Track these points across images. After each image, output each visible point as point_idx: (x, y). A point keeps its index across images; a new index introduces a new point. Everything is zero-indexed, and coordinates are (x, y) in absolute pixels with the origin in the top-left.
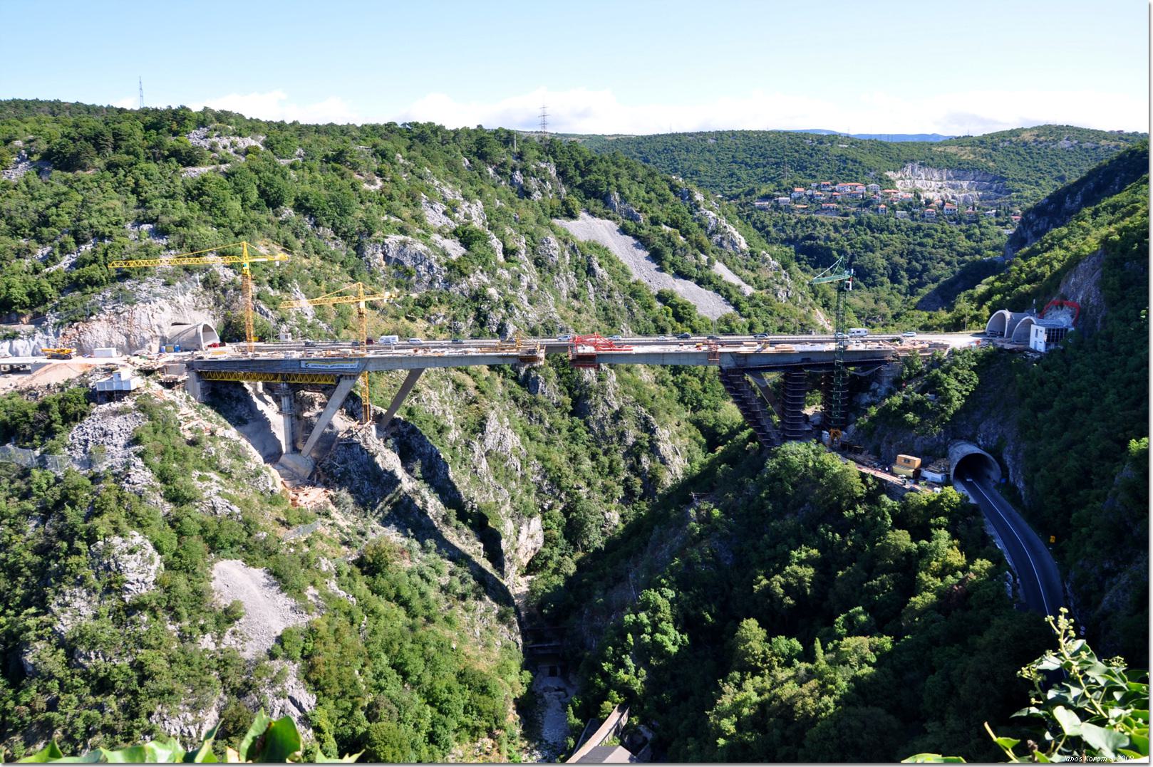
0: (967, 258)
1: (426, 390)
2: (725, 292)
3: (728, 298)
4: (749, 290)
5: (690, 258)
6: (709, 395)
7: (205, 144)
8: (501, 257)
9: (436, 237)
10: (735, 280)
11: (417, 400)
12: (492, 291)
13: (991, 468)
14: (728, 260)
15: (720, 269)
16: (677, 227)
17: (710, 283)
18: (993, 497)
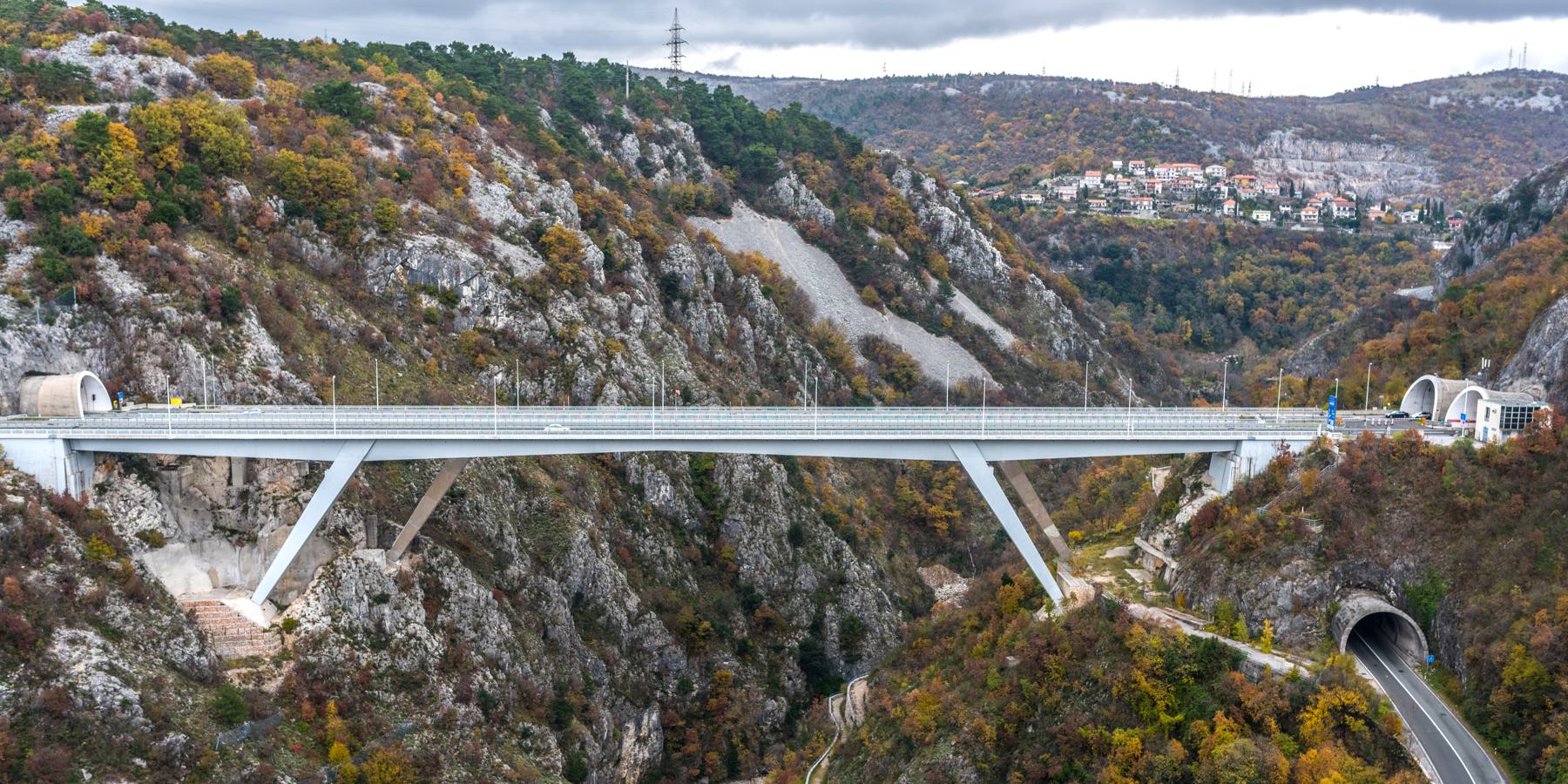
2: (975, 342)
4: (1006, 339)
7: (94, 66)
10: (985, 322)
12: (585, 333)
15: (962, 303)
18: (1415, 687)
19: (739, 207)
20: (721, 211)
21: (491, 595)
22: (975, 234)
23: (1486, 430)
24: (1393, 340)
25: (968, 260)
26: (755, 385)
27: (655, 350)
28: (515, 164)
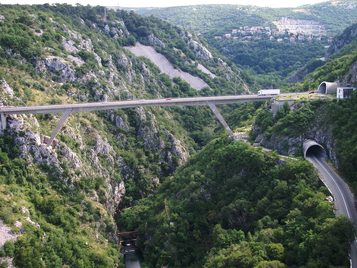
1: (68, 127)
3: (204, 79)
4: (213, 76)
5: (187, 63)
6: (198, 124)
8: (100, 65)
9: (71, 57)
11: (65, 132)
14: (204, 63)
15: (200, 67)
16: (181, 49)
17: (196, 73)
19: (138, 44)
20: (132, 44)
21: (76, 155)
22: (204, 49)
23: (339, 95)
24: (315, 73)
25: (202, 55)
26: (145, 92)
27: (116, 84)
28: (75, 35)
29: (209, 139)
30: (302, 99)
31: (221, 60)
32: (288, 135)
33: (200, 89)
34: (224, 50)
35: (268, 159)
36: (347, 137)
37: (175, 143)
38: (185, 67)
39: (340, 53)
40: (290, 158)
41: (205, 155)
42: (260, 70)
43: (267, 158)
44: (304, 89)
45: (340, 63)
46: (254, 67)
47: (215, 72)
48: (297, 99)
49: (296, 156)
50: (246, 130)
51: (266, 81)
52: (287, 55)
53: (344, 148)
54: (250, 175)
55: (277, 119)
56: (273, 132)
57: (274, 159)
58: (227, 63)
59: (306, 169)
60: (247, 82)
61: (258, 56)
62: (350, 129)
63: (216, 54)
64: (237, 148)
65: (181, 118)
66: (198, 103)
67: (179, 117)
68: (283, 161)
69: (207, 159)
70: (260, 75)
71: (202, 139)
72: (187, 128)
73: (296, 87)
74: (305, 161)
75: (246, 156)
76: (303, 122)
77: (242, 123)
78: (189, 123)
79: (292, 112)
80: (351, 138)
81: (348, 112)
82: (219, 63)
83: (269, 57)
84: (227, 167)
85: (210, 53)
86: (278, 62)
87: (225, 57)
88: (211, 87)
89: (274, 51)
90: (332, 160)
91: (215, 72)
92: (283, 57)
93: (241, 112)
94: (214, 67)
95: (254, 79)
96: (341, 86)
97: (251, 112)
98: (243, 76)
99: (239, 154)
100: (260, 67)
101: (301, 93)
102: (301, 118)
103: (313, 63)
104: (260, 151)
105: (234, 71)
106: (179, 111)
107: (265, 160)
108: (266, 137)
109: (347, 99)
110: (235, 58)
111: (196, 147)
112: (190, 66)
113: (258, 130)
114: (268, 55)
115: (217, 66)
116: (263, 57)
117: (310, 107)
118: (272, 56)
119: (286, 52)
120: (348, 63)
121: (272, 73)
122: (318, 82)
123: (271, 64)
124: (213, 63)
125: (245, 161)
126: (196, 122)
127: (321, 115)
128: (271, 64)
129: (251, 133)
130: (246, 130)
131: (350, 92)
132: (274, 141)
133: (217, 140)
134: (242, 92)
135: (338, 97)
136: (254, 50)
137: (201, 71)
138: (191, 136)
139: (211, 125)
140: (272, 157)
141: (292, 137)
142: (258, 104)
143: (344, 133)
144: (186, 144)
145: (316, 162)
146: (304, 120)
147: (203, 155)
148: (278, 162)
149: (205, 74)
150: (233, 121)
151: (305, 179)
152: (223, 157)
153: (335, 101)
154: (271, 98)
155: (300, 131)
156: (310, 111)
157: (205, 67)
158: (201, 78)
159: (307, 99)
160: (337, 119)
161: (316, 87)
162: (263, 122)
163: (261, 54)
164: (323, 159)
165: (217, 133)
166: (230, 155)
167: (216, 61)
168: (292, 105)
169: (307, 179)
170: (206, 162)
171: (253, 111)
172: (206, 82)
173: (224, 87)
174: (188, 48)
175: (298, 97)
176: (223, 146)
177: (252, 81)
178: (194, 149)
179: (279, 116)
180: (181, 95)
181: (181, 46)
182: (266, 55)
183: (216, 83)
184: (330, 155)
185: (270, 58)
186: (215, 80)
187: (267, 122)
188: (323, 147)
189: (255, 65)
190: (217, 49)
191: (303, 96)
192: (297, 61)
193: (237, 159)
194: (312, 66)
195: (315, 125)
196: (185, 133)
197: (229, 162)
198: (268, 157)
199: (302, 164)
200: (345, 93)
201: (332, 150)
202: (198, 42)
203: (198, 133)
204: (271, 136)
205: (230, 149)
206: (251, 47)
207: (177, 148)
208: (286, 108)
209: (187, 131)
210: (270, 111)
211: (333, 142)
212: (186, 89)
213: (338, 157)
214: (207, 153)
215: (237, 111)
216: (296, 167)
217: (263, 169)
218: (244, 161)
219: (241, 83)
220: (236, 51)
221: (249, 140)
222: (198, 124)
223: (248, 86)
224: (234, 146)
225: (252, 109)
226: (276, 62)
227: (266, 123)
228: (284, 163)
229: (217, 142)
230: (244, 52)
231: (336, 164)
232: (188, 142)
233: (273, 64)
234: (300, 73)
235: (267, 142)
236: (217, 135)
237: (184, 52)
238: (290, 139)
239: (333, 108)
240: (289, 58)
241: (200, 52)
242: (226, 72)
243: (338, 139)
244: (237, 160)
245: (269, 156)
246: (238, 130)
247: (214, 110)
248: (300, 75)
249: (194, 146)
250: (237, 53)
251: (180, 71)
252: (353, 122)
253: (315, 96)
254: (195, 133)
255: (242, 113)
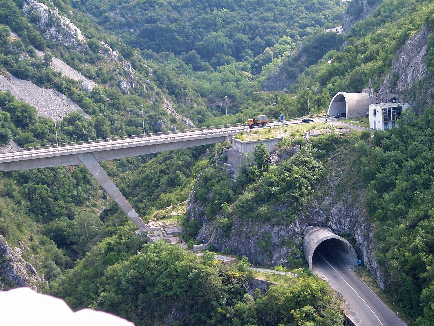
0: (308, 30)
3: (70, 96)
4: (90, 85)
5: (24, 57)
6: (61, 202)
10: (74, 75)
13: (347, 252)
14: (66, 55)
15: (58, 65)
16: (7, 23)
17: (49, 80)
22: (65, 21)
23: (375, 122)
24: (323, 67)
25: (60, 36)
29: (92, 237)
30: (293, 135)
31: (107, 46)
32: (269, 221)
33: (60, 119)
34: (112, 19)
35: (228, 280)
36: (397, 217)
37: (8, 256)
38: (20, 68)
39: (373, 19)
40: (277, 273)
41: (82, 281)
42: (200, 60)
43: (227, 278)
44: (299, 110)
45: (373, 47)
46: (184, 55)
47: (94, 74)
48: (284, 136)
49: (290, 266)
50: (174, 213)
51: (215, 87)
52: (259, 23)
53: (392, 243)
54: (190, 320)
55: (242, 185)
56: (235, 217)
57: (243, 279)
58: (122, 51)
59: (313, 296)
60: (172, 93)
61: (193, 28)
62: (401, 197)
63: (93, 31)
64: (156, 259)
65: (20, 192)
66: (60, 161)
67: (14, 190)
68: (262, 282)
69: (88, 291)
70: (199, 73)
71: (73, 239)
72: (37, 215)
73: (281, 106)
74: (310, 278)
75: (178, 276)
76: (299, 188)
77: (165, 197)
78: (40, 201)
79: (275, 167)
80: (406, 218)
81: (394, 161)
82: (101, 54)
83: (218, 30)
84: (137, 307)
85: (78, 30)
86: (239, 41)
87: (114, 38)
88: (87, 112)
89: (227, 16)
90: (369, 270)
91: (94, 74)
92: (250, 30)
93: (160, 167)
94: (92, 62)
95: (186, 85)
96: (378, 100)
97: (184, 169)
98: (160, 79)
99: (162, 273)
100: (198, 54)
101: (291, 122)
102: (296, 179)
103: (317, 41)
104: (209, 262)
105: (139, 71)
106: (14, 174)
107: (223, 282)
108: (221, 227)
109: (391, 132)
110: (139, 36)
111: (61, 259)
112: (32, 65)
113: (203, 214)
114: (215, 25)
115: (99, 59)
116: (203, 30)
117: (312, 153)
118: (224, 27)
119: (257, 15)
120: (389, 47)
121: (226, 67)
122: (328, 92)
123: (223, 45)
124: (87, 54)
125: (178, 289)
126: (56, 199)
127: (338, 169)
128: (223, 45)
129: (186, 221)
130: (174, 213)
131: (397, 115)
132: (240, 237)
133: (109, 244)
134: (160, 119)
135: (371, 126)
136: (182, 15)
137: (60, 74)
138: (47, 233)
139: (93, 202)
140: (237, 275)
141: (278, 224)
142: (198, 151)
143: (391, 207)
144: (37, 254)
145: (335, 277)
146: (301, 184)
147: (79, 280)
148: (251, 284)
149: (70, 82)
150: (145, 190)
151: (314, 319)
152: (127, 282)
153: (365, 136)
154: (225, 137)
155: (296, 210)
156: (315, 163)
157: (69, 64)
158: (62, 92)
159: (305, 135)
160: (372, 176)
161: (325, 104)
162: (211, 195)
163: (198, 23)
164: (350, 269)
165: (108, 223)
166: (143, 277)
167: (93, 47)
168: (273, 152)
169: (318, 318)
170: (88, 296)
171: (188, 166)
172: (74, 101)
173: (118, 109)
174: (24, 20)
175: (285, 132)
176: (124, 256)
177: (182, 90)
178: (57, 264)
179: (248, 178)
180: (15, 135)
181: (7, 17)
182: (212, 26)
183: (97, 101)
184: (366, 259)
185: (221, 33)
186: (94, 94)
187: (221, 194)
188: (348, 243)
189: (187, 52)
190: (95, 16)
191: (296, 130)
192: (282, 37)
193: (159, 284)
194: (315, 48)
195: (326, 194)
196: (32, 229)
197: (141, 295)
198: (228, 276)
199: (305, 286)
200: (386, 116)
201: (368, 247)
202: (48, 5)
203: (64, 224)
204: (232, 224)
205: (141, 263)
206: (175, 8)
207: (15, 266)
208: (261, 159)
209: (37, 221)
210: (226, 167)
211: (369, 228)
212: (28, 120)
213: (382, 263)
214: (87, 277)
215: (152, 167)
216: (291, 293)
217: (221, 305)
218: (176, 289)
219: (157, 97)
220: (139, 20)
221: (183, 237)
222: (61, 202)
223: (175, 102)
224: (150, 256)
225: (187, 160)
226: (234, 41)
227: (218, 197)
228: (265, 287)
229: (110, 248)
230: (159, 20)
231: (379, 278)
232: (41, 250)
233: (229, 46)
234: (290, 65)
235: (224, 240)
236: (108, 226)
237: (15, 31)
238: (276, 229)
239: (363, 152)
240: (264, 29)
241: (54, 29)
242: (120, 74)
243: (378, 223)
244: (159, 288)
245: (230, 273)
246: (156, 216)
247: (97, 173)
248: (291, 69)
249: (55, 257)
250: (142, 25)
251: (8, 77)
252: (407, 183)
253: (322, 125)
254: (56, 224)
255: (162, 171)
